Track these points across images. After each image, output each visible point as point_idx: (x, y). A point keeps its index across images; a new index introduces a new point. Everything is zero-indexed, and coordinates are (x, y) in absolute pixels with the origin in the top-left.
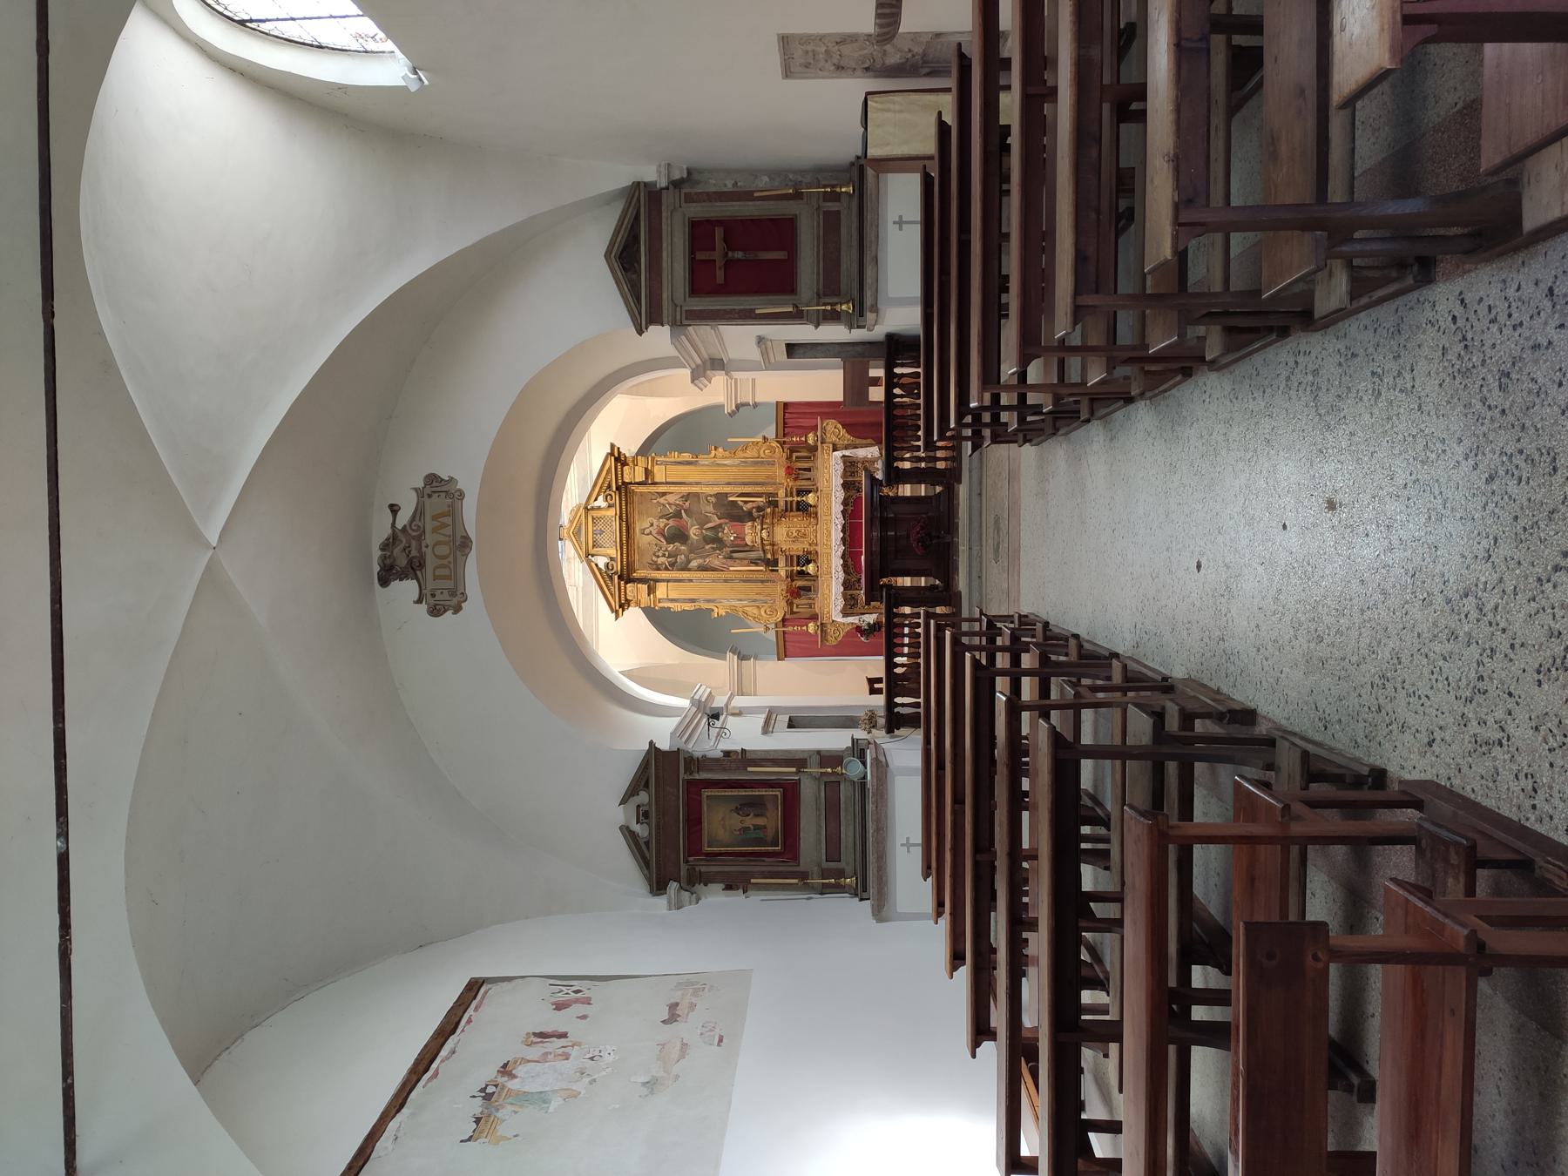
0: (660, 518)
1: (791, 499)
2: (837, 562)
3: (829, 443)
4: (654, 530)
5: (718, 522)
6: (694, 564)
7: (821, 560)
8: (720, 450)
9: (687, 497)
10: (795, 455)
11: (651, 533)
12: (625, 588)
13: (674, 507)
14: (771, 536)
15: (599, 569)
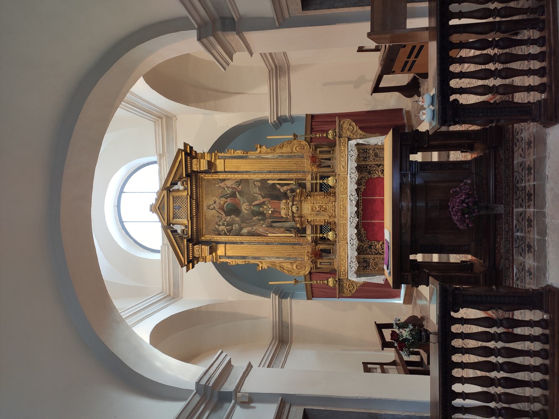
0: (221, 197)
1: (315, 181)
2: (351, 232)
3: (345, 137)
6: (245, 231)
7: (339, 229)
8: (264, 148)
9: (240, 182)
10: (319, 150)
11: (214, 208)
13: (230, 190)
14: (299, 210)
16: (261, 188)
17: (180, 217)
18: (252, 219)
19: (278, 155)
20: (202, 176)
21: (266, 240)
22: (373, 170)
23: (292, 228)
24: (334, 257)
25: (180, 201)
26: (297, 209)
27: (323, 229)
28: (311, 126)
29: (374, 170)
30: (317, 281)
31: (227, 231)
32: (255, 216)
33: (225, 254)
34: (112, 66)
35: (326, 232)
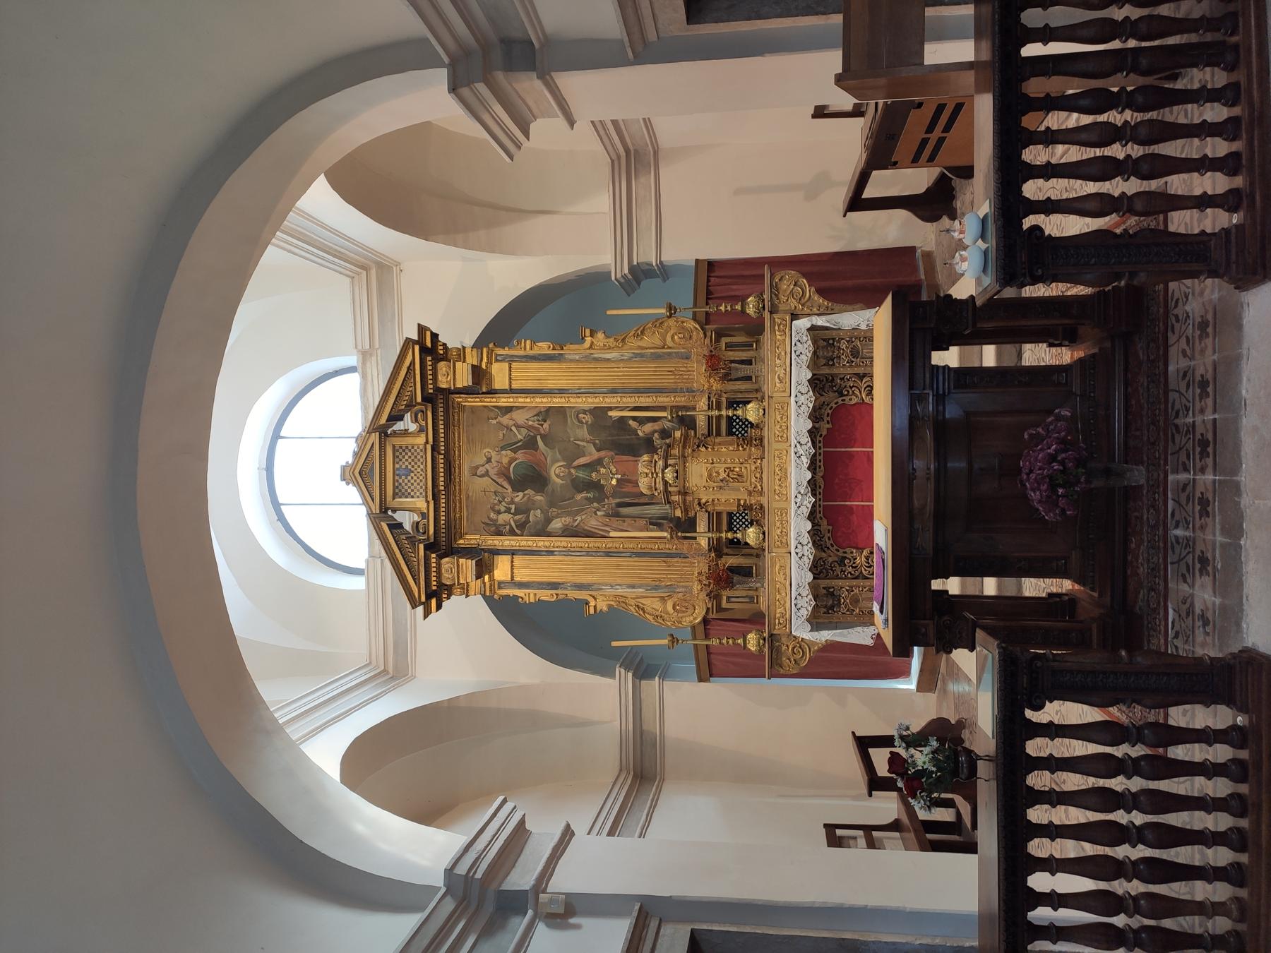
0: (503, 448)
6: (557, 524)
11: (487, 474)
16: (592, 428)
17: (409, 494)
18: (573, 497)
19: (633, 353)
20: (459, 400)
21: (604, 546)
23: (663, 518)
24: (758, 585)
25: (410, 457)
26: (675, 475)
27: (735, 521)
28: (708, 286)
29: (851, 388)
30: (720, 639)
33: (512, 577)
35: (741, 529)
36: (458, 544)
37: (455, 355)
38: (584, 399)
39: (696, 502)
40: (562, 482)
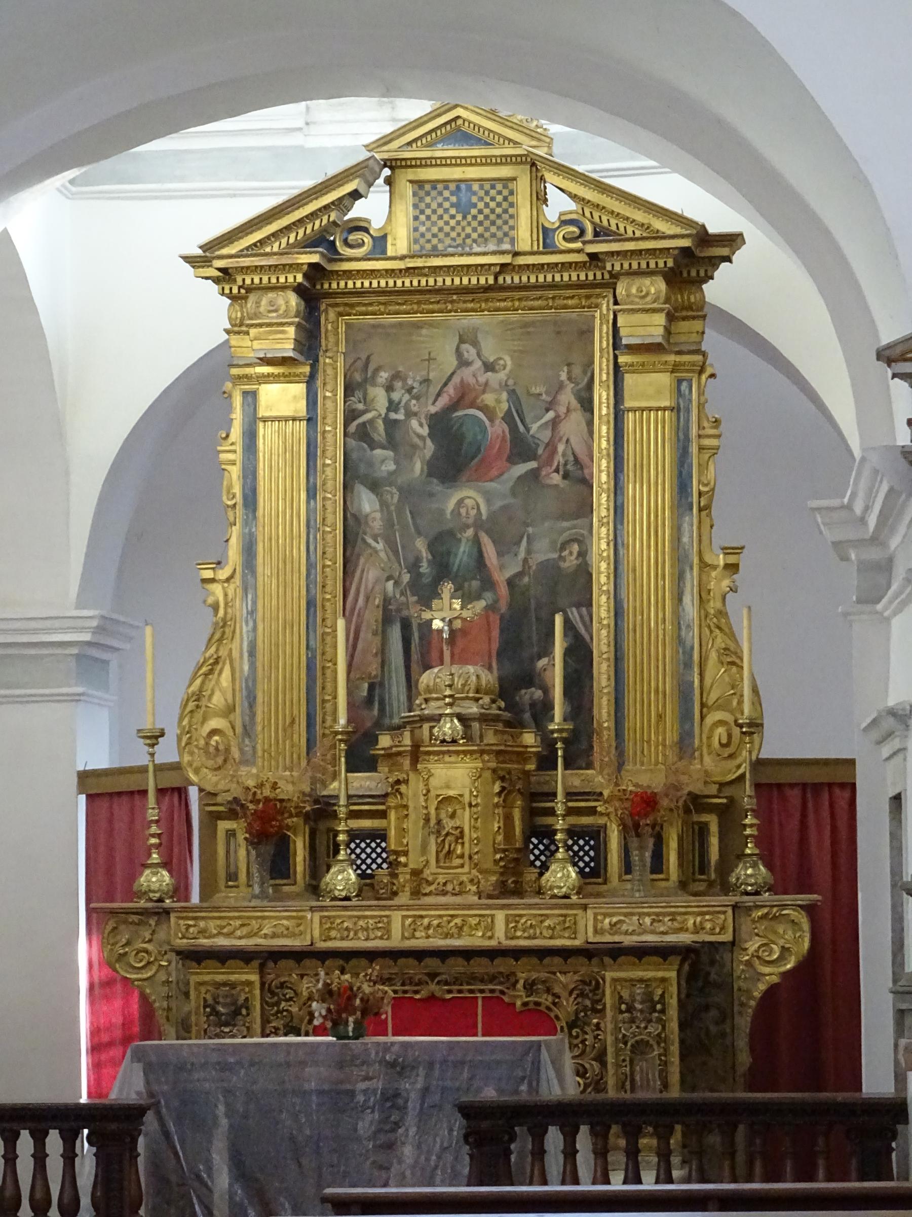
0: (512, 393)
4: (473, 374)
5: (501, 577)
6: (367, 502)
11: (463, 363)
12: (283, 288)
15: (342, 204)
16: (550, 571)
17: (422, 212)
18: (419, 533)
19: (692, 648)
20: (604, 307)
21: (328, 596)
22: (587, 1037)
23: (382, 710)
24: (257, 889)
25: (493, 211)
26: (448, 739)
27: (368, 845)
28: (830, 785)
29: (583, 1042)
30: (157, 822)
31: (364, 424)
32: (431, 547)
33: (265, 420)
34: (768, 222)
35: (353, 856)
36: (326, 311)
37: (689, 299)
38: (605, 554)
39: (402, 776)
40: (449, 511)
